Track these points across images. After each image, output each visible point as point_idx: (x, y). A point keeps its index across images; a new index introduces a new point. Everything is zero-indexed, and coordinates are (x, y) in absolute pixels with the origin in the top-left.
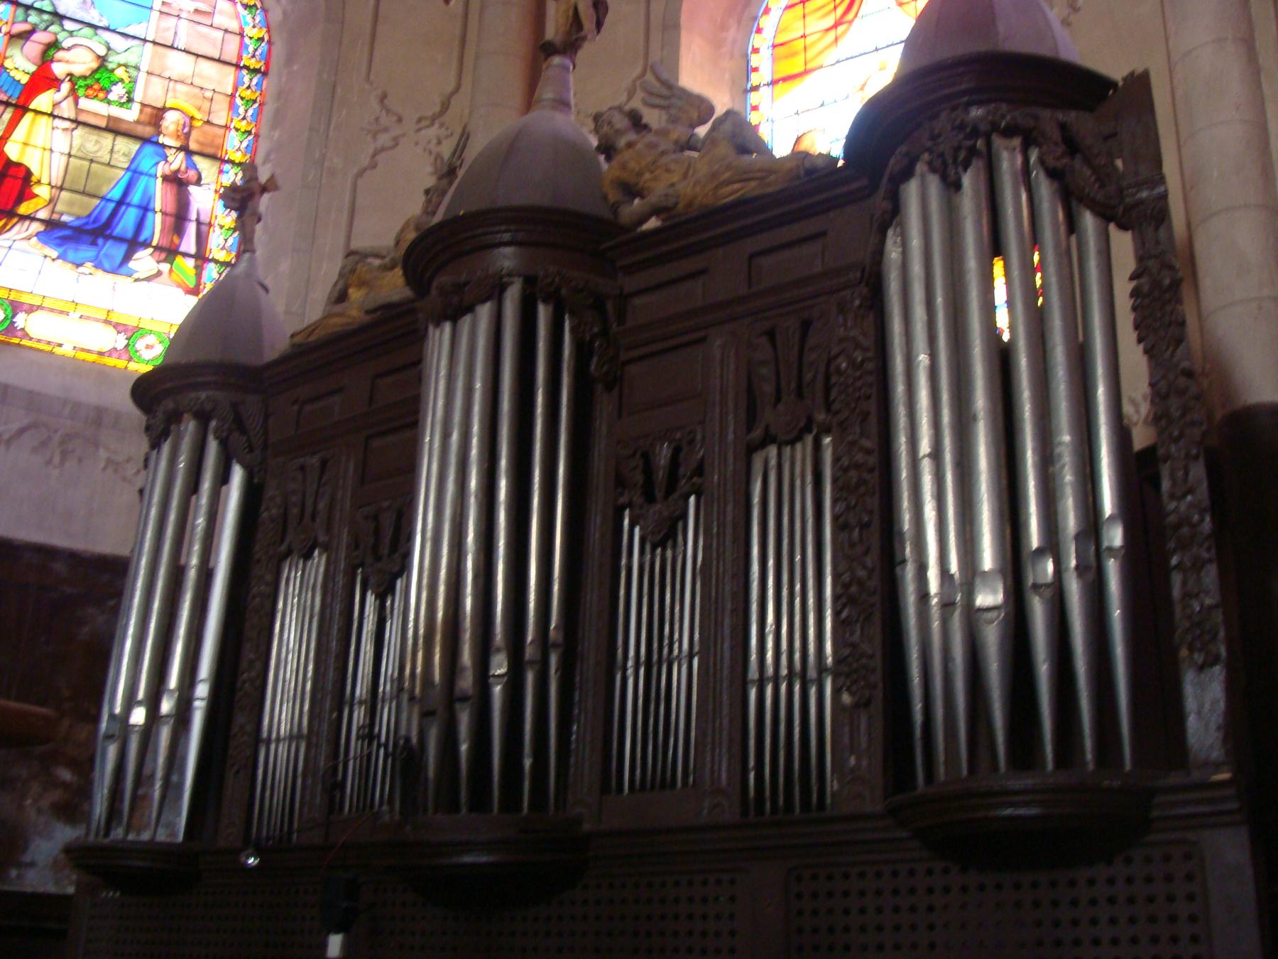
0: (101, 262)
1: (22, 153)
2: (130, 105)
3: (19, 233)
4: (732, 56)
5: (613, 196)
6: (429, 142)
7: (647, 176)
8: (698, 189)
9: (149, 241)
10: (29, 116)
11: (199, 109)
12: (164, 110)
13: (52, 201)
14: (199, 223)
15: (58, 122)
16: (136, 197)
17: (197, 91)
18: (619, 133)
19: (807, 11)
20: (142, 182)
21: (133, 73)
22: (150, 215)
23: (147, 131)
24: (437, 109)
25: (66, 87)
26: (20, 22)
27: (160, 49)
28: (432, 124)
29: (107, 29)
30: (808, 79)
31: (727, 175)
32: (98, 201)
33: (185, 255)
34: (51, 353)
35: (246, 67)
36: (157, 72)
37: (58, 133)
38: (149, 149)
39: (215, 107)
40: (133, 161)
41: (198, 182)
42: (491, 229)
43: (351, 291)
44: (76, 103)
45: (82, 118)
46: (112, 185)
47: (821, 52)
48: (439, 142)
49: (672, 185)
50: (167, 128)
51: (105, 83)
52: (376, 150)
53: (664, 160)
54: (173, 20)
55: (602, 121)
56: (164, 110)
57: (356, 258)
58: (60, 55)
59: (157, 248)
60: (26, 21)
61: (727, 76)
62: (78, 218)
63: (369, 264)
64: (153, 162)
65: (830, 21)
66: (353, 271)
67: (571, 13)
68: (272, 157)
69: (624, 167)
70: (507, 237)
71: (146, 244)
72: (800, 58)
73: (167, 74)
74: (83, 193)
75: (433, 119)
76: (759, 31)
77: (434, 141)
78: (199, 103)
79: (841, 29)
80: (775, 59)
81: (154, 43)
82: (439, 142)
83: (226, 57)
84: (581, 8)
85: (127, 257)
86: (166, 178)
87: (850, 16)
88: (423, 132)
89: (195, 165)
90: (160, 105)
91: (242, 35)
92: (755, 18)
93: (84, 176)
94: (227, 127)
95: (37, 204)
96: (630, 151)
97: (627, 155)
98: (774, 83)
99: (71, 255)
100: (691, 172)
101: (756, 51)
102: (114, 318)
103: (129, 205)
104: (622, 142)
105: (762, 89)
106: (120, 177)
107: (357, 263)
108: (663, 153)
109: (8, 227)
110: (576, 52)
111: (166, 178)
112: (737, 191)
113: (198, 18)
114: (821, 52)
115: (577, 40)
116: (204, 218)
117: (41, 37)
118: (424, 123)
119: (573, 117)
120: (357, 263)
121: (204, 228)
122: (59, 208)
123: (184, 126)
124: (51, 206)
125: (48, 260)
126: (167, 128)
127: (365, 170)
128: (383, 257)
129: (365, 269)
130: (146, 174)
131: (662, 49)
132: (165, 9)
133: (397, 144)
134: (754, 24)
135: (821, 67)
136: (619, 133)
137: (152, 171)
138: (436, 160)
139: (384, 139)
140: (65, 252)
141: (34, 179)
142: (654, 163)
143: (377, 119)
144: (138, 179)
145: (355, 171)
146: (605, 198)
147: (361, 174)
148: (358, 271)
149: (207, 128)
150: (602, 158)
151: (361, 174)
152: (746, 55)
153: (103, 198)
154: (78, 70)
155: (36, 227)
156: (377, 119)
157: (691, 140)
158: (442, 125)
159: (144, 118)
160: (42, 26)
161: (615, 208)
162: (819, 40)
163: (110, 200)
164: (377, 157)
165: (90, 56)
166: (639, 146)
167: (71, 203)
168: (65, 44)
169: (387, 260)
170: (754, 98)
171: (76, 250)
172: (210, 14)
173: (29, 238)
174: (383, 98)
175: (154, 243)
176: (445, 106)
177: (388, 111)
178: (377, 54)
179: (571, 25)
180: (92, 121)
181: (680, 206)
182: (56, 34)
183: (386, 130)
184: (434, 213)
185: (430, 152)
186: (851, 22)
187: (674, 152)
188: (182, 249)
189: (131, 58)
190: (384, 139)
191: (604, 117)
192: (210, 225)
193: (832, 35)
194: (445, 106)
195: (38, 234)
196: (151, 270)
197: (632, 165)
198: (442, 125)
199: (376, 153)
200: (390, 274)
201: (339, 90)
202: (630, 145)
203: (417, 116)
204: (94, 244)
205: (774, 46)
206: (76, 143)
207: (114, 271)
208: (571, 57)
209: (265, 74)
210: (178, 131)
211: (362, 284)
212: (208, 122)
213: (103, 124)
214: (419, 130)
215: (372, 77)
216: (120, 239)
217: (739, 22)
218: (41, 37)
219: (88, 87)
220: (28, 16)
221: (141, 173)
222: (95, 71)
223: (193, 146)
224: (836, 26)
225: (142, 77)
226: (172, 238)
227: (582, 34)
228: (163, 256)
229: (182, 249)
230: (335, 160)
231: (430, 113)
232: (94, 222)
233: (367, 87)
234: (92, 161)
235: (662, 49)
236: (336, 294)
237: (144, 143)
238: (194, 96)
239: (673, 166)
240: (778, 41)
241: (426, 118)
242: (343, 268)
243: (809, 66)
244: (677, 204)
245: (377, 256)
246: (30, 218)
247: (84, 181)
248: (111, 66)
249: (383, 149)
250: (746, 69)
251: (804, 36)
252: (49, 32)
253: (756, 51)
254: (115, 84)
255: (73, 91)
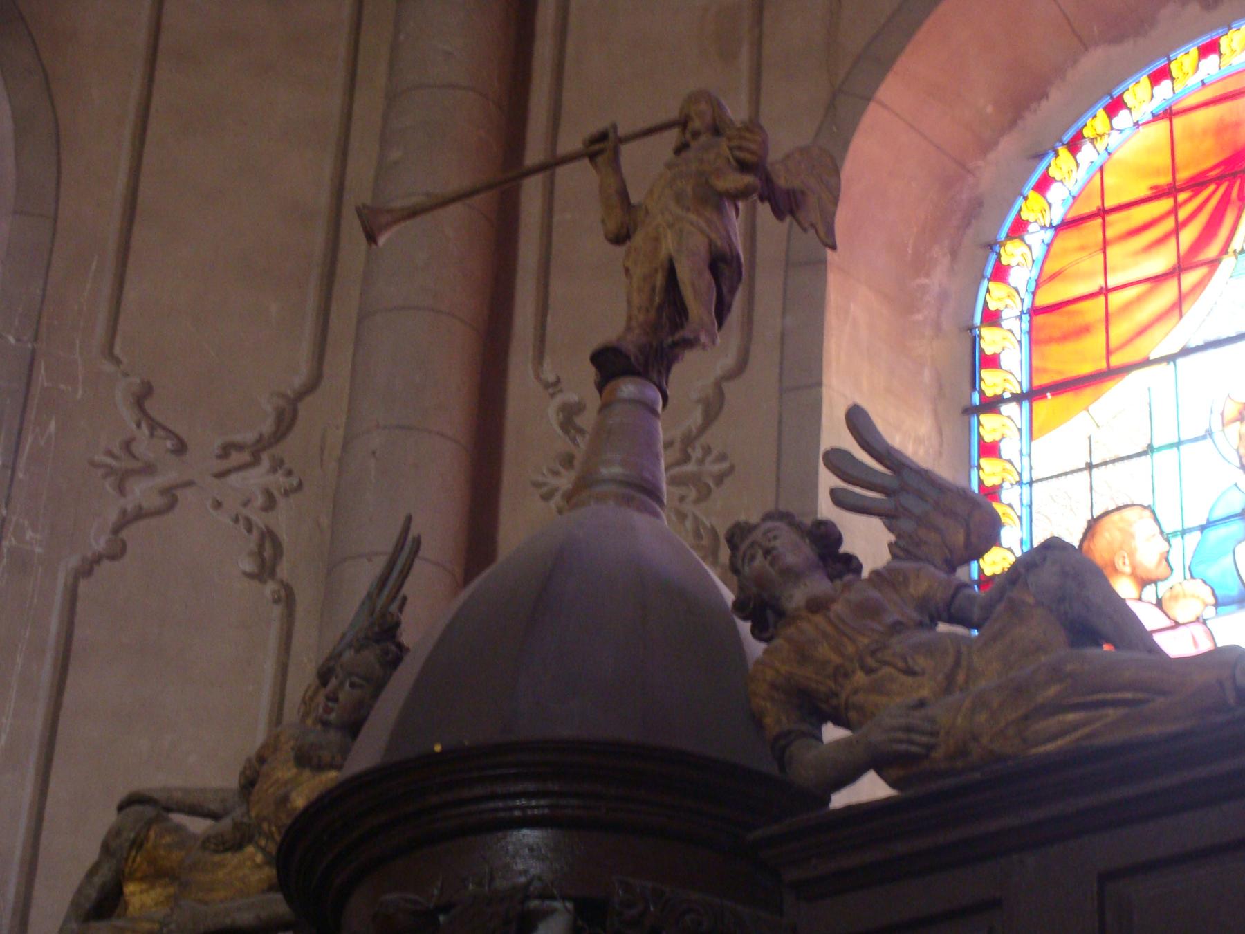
4: (938, 327)
5: (776, 719)
6: (246, 504)
7: (860, 678)
8: (982, 717)
18: (792, 575)
19: (1110, 233)
24: (267, 427)
28: (256, 461)
30: (1116, 391)
31: (1052, 691)
42: (500, 789)
43: (130, 888)
47: (1142, 331)
48: (270, 503)
49: (921, 704)
52: (124, 512)
53: (897, 644)
55: (753, 544)
57: (149, 811)
61: (927, 376)
63: (179, 828)
65: (1163, 260)
66: (137, 844)
67: (660, 280)
69: (803, 654)
70: (538, 807)
72: (1095, 343)
75: (257, 450)
76: (1000, 273)
77: (260, 500)
79: (1189, 279)
80: (1035, 340)
82: (270, 503)
84: (684, 273)
87: (1212, 251)
88: (234, 479)
92: (991, 246)
96: (818, 619)
97: (810, 627)
98: (1033, 394)
100: (961, 678)
101: (992, 318)
104: (796, 597)
105: (1005, 409)
107: (149, 824)
108: (897, 628)
110: (668, 369)
112: (1075, 727)
114: (1142, 331)
115: (675, 345)
118: (236, 458)
119: (666, 518)
120: (149, 824)
127: (98, 559)
128: (215, 816)
129: (168, 839)
131: (784, 314)
133: (172, 504)
134: (987, 259)
135: (1146, 362)
136: (792, 575)
138: (261, 546)
139: (142, 491)
142: (873, 653)
143: (127, 445)
145: (74, 561)
146: (757, 721)
147: (87, 569)
148: (149, 845)
150: (745, 627)
151: (87, 569)
152: (971, 328)
156: (127, 445)
157: (960, 596)
158: (277, 465)
161: (780, 747)
162: (1139, 299)
164: (124, 534)
166: (838, 608)
169: (226, 824)
170: (989, 426)
174: (142, 397)
176: (286, 421)
177: (154, 425)
178: (131, 295)
179: (660, 308)
181: (938, 754)
183: (149, 469)
184: (353, 728)
185: (249, 527)
186: (1213, 264)
187: (920, 625)
190: (142, 491)
191: (757, 535)
193: (1168, 293)
194: (286, 421)
197: (824, 651)
198: (277, 465)
199: (126, 520)
200: (232, 859)
201: (42, 376)
202: (817, 606)
203: (219, 442)
205: (1035, 311)
208: (655, 377)
211: (156, 874)
214: (221, 475)
215: (117, 350)
217: (954, 254)
224: (1176, 272)
227: (686, 333)
230: (29, 534)
231: (249, 437)
233: (108, 367)
235: (784, 314)
236: (93, 893)
239: (921, 662)
240: (1045, 299)
241: (240, 447)
242: (115, 832)
243: (1116, 360)
244: (930, 748)
245: (194, 811)
249: (140, 514)
250: (968, 360)
251: (1105, 291)
253: (992, 318)
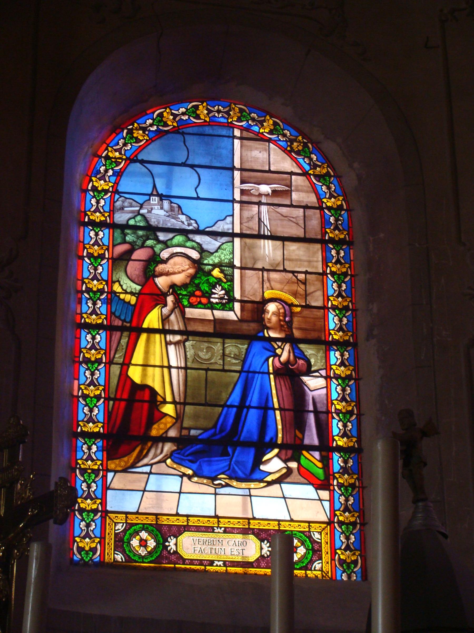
0: (234, 471)
1: (144, 375)
2: (231, 305)
3: (155, 456)
9: (274, 440)
10: (144, 337)
11: (295, 294)
12: (265, 302)
13: (179, 418)
14: (316, 412)
15: (170, 338)
16: (254, 399)
17: (291, 275)
20: (258, 381)
21: (228, 270)
22: (270, 412)
23: (252, 327)
25: (170, 299)
26: (120, 244)
27: (248, 241)
29: (198, 232)
32: (220, 409)
33: (310, 448)
34: (205, 571)
35: (331, 240)
36: (250, 266)
37: (172, 349)
38: (257, 346)
39: (310, 289)
40: (244, 361)
41: (309, 372)
44: (183, 313)
45: (192, 327)
46: (230, 390)
50: (269, 319)
51: (205, 287)
54: (255, 208)
56: (265, 302)
58: (161, 267)
59: (281, 447)
60: (124, 242)
62: (205, 430)
64: (264, 358)
68: (375, 332)
71: (272, 445)
73: (259, 266)
74: (206, 404)
78: (295, 287)
81: (242, 235)
83: (310, 235)
85: (258, 461)
86: (277, 373)
89: (302, 352)
90: (258, 299)
91: (320, 208)
93: (203, 383)
94: (324, 308)
95: (165, 424)
99: (206, 470)
102: (254, 525)
103: (250, 407)
106: (235, 379)
109: (145, 452)
111: (277, 373)
113: (276, 200)
116: (322, 408)
117: (140, 254)
121: (323, 417)
122: (186, 424)
123: (285, 316)
124: (178, 425)
125: (185, 479)
126: (269, 319)
130: (259, 373)
132: (245, 198)
137: (264, 369)
140: (200, 467)
141: (159, 399)
144: (253, 378)
149: (306, 312)
153: (223, 406)
154: (178, 279)
155: (168, 447)
159: (247, 315)
160: (139, 243)
163: (232, 406)
165: (185, 263)
167: (196, 417)
168: (165, 254)
171: (210, 463)
172: (288, 193)
173: (163, 461)
175: (279, 441)
180: (200, 328)
182: (152, 247)
188: (307, 442)
189: (223, 256)
192: (328, 412)
195: (171, 455)
196: (254, 356)
204: (225, 454)
206: (190, 353)
207: (247, 479)
209: (350, 244)
210: (280, 320)
212: (307, 307)
213: (210, 329)
216: (247, 444)
218: (140, 254)
219: (192, 295)
220: (125, 235)
221: (255, 372)
222: (193, 277)
223: (297, 334)
225: (237, 273)
226: (295, 432)
228: (290, 453)
229: (307, 442)
232: (222, 430)
234: (207, 370)
237: (329, 501)
238: (289, 282)
246: (164, 439)
247: (203, 392)
248: (208, 268)
252: (147, 247)
254: (214, 287)
255: (178, 305)
